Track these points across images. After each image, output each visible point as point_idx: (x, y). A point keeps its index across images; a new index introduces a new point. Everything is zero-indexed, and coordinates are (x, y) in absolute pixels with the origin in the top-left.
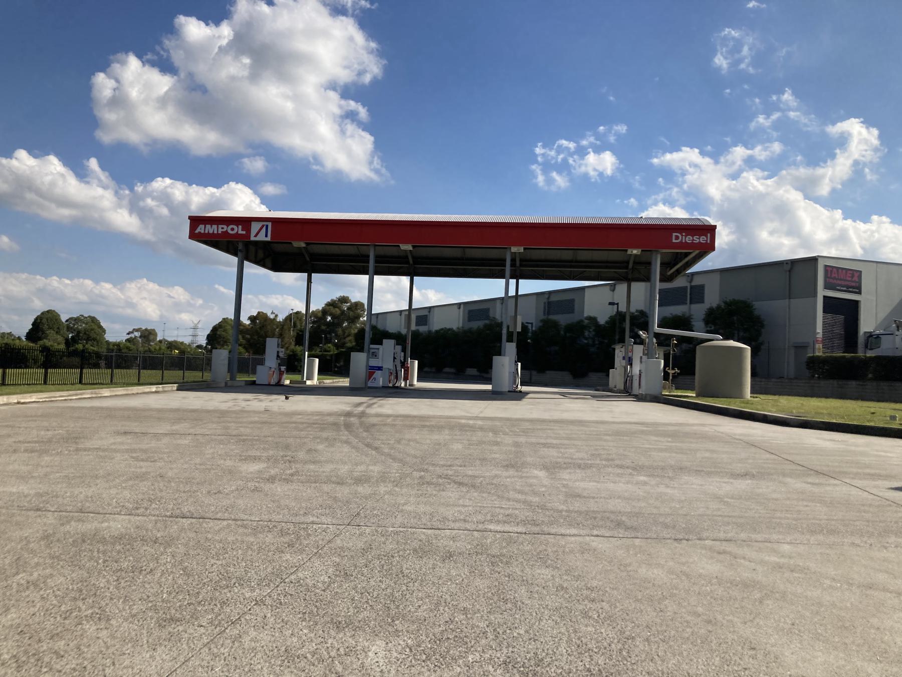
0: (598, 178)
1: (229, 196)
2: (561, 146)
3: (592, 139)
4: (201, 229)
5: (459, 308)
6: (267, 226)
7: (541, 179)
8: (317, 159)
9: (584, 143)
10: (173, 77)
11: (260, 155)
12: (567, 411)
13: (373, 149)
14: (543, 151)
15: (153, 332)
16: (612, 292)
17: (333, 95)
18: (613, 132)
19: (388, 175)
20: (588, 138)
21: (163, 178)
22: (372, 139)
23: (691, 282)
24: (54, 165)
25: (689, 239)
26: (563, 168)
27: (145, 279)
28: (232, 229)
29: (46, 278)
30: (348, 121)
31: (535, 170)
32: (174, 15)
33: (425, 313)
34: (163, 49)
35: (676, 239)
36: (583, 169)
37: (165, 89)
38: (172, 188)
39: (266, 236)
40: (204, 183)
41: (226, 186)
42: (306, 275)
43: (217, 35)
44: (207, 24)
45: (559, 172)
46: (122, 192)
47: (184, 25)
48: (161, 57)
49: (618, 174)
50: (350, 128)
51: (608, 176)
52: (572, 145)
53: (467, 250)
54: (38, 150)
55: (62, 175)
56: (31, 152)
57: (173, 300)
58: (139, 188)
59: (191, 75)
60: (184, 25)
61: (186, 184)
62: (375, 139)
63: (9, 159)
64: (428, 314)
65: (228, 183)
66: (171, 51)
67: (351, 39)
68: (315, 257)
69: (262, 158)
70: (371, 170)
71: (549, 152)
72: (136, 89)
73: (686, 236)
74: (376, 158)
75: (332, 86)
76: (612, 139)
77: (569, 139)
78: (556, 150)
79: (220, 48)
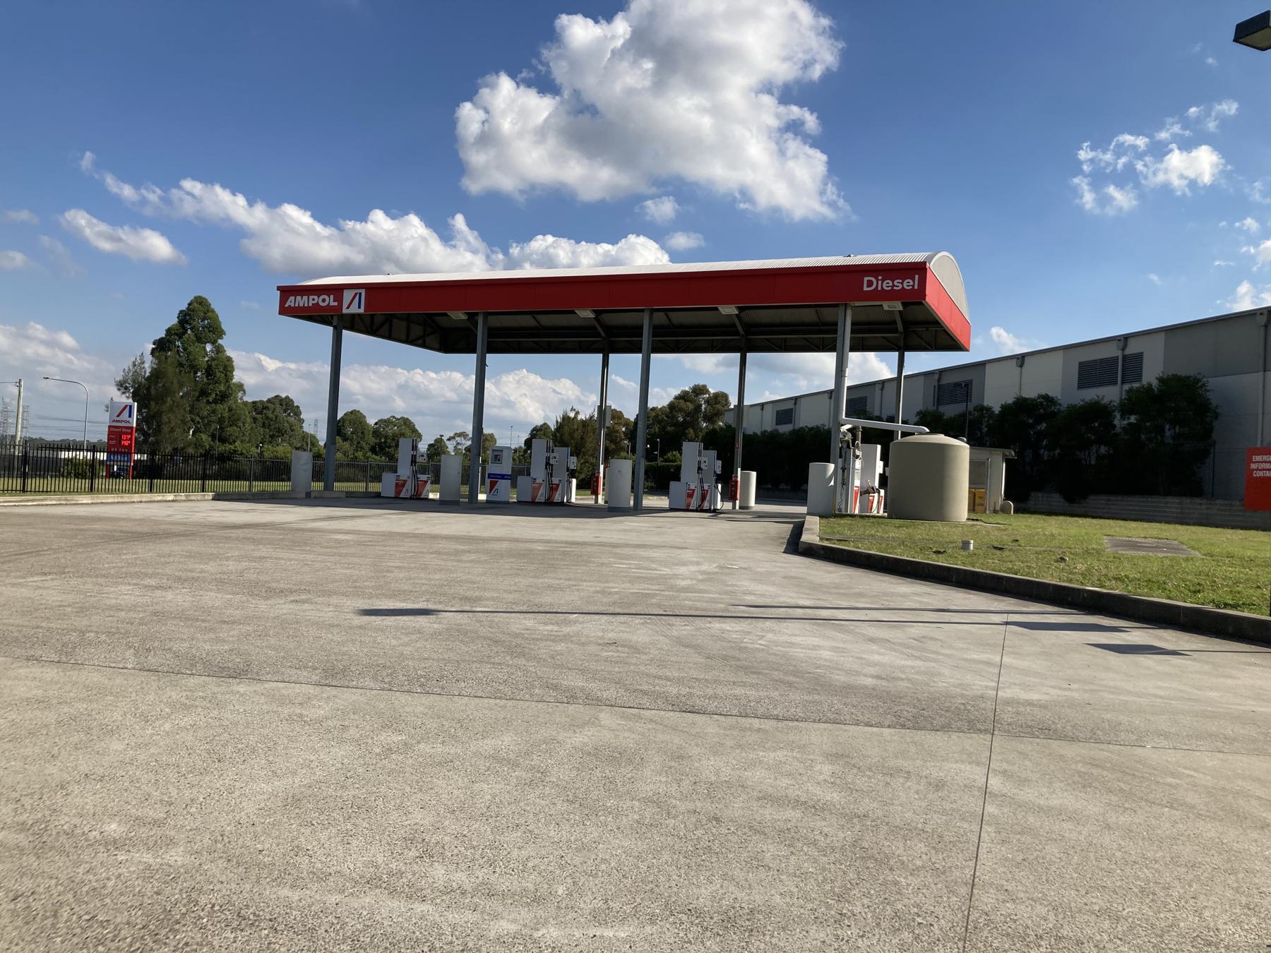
0: (1186, 189)
1: (627, 253)
2: (1123, 144)
3: (1176, 129)
4: (291, 302)
5: (830, 398)
6: (360, 294)
7: (1088, 198)
8: (745, 194)
9: (1163, 135)
10: (554, 98)
11: (667, 194)
12: (503, 525)
13: (826, 173)
14: (1091, 155)
15: (489, 438)
16: (1019, 369)
17: (767, 100)
18: (1213, 114)
19: (848, 208)
20: (1168, 127)
21: (544, 235)
22: (824, 158)
23: (1123, 349)
24: (415, 226)
25: (887, 285)
26: (1127, 178)
27: (525, 370)
28: (324, 300)
29: (408, 372)
30: (790, 135)
31: (1079, 185)
32: (555, 16)
33: (790, 405)
34: (541, 62)
35: (868, 286)
36: (1161, 178)
37: (545, 114)
38: (555, 248)
39: (359, 307)
40: (595, 238)
41: (623, 240)
42: (737, 356)
43: (609, 35)
44: (597, 22)
45: (1120, 185)
46: (494, 256)
47: (568, 26)
48: (538, 73)
49: (1223, 181)
50: (793, 145)
51: (1205, 185)
52: (1141, 142)
53: (825, 310)
54: (396, 211)
55: (424, 239)
56: (388, 213)
57: (559, 396)
58: (515, 251)
59: (576, 93)
60: (568, 26)
61: (573, 241)
62: (829, 157)
63: (363, 223)
64: (793, 407)
65: (626, 237)
66: (551, 64)
67: (793, 17)
68: (751, 328)
69: (671, 198)
70: (822, 203)
71: (1101, 156)
72: (509, 120)
73: (883, 281)
74: (830, 185)
75: (767, 88)
76: (1212, 126)
77: (1136, 132)
78: (1113, 151)
79: (613, 52)
